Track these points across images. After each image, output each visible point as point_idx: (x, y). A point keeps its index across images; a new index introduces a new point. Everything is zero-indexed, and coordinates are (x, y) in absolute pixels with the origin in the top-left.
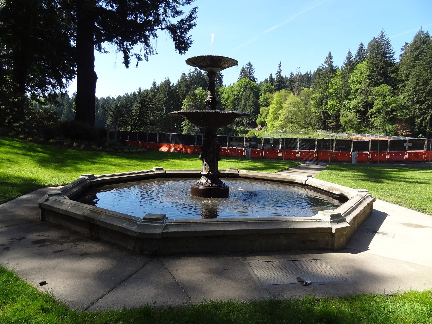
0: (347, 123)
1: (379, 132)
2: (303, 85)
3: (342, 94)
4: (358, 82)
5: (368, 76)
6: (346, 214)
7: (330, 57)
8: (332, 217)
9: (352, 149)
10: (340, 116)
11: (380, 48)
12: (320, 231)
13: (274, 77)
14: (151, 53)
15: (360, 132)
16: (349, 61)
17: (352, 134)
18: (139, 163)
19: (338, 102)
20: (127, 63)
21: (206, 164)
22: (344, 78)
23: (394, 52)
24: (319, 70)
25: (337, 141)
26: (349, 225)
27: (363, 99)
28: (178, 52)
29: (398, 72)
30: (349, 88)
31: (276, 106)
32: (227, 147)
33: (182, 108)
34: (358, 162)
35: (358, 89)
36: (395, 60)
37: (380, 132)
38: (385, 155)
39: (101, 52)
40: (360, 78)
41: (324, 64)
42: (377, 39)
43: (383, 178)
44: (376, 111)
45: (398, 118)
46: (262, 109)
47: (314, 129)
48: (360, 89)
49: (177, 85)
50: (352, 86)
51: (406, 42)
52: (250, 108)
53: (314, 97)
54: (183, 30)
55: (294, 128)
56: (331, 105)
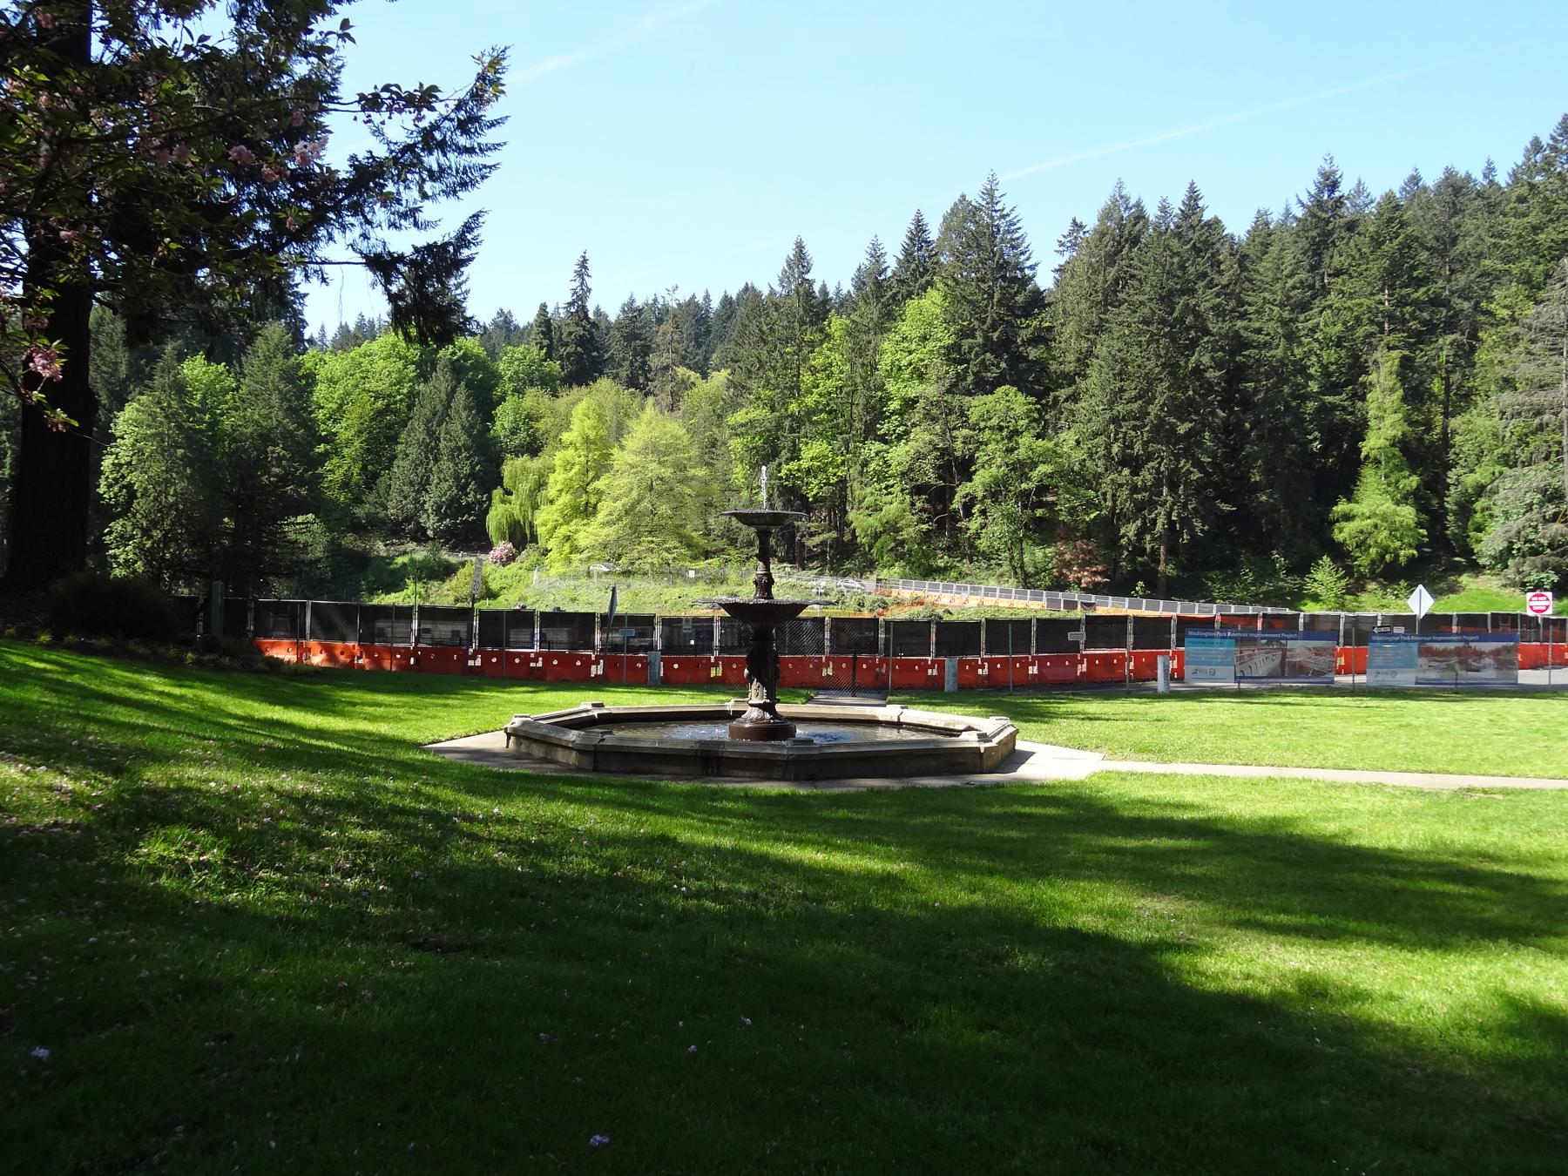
0: (877, 536)
5: (950, 349)
9: (933, 648)
11: (984, 242)
15: (929, 572)
22: (860, 350)
23: (1036, 265)
27: (936, 440)
31: (583, 459)
33: (112, 454)
35: (915, 401)
37: (1001, 575)
38: (1026, 665)
46: (510, 467)
47: (748, 559)
50: (891, 387)
51: (1074, 221)
52: (452, 458)
55: (665, 554)
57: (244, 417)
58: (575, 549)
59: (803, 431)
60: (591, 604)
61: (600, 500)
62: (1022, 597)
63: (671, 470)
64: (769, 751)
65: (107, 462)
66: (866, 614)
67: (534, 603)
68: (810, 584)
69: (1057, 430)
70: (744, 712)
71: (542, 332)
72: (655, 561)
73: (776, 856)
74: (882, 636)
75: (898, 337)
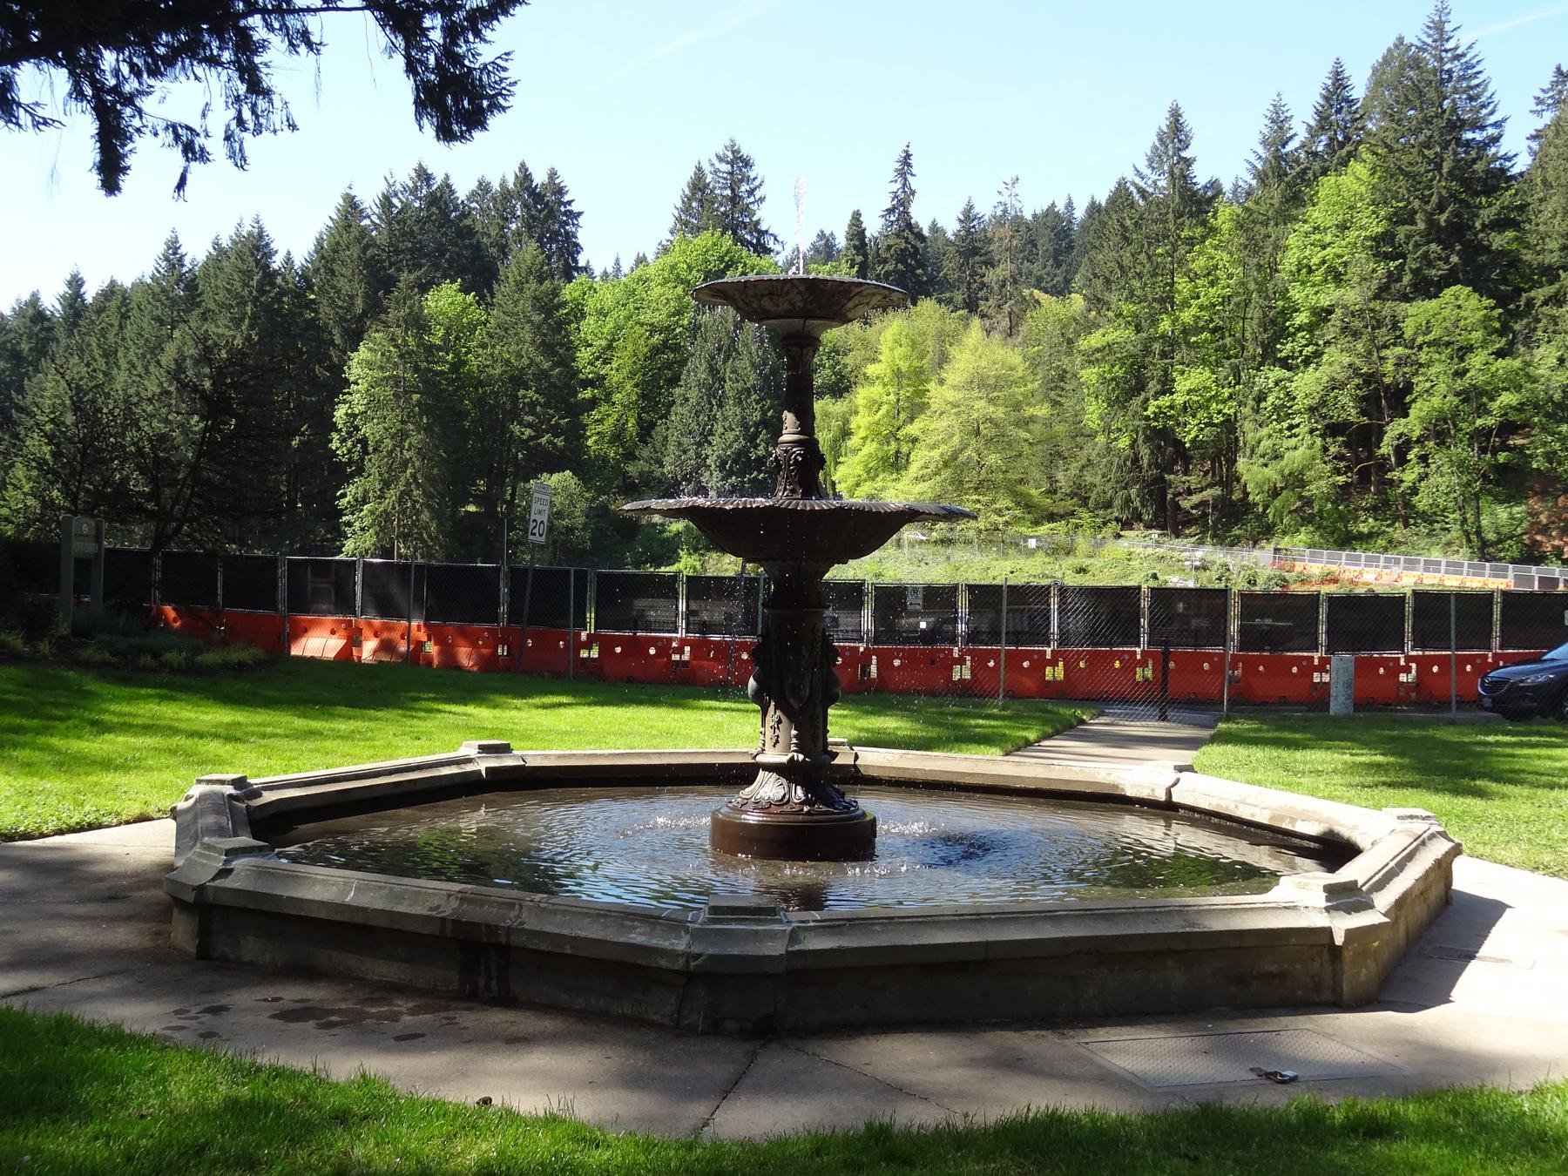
0: (1275, 493)
1: (1444, 540)
2: (1030, 273)
3: (1248, 335)
4: (1328, 272)
5: (1378, 240)
6: (1372, 886)
7: (1176, 133)
8: (1332, 891)
9: (1323, 638)
10: (1237, 451)
11: (1431, 94)
12: (1293, 941)
13: (873, 226)
14: (262, 120)
15: (1346, 541)
16: (1279, 158)
18: (300, 723)
19: (1226, 379)
20: (111, 170)
21: (779, 722)
22: (1254, 247)
23: (1504, 120)
24: (1121, 196)
25: (1254, 603)
26: (1387, 920)
27: (1358, 362)
28: (429, 130)
29: (1527, 227)
30: (1281, 303)
31: (892, 398)
33: (345, 402)
34: (1358, 706)
35: (1329, 311)
36: (1509, 159)
37: (1449, 544)
39: (10, 125)
40: (1339, 251)
41: (1146, 171)
42: (1413, 49)
43: (1483, 776)
44: (1425, 429)
45: (1538, 470)
47: (1105, 524)
48: (1339, 312)
49: (312, 262)
50: (1297, 293)
51: (1558, 68)
53: (1098, 350)
54: (457, 17)
55: (995, 518)
56: (1189, 392)
57: (492, 355)
59: (1178, 357)
65: (340, 413)
69: (1530, 343)
71: (855, 247)
75: (1307, 227)
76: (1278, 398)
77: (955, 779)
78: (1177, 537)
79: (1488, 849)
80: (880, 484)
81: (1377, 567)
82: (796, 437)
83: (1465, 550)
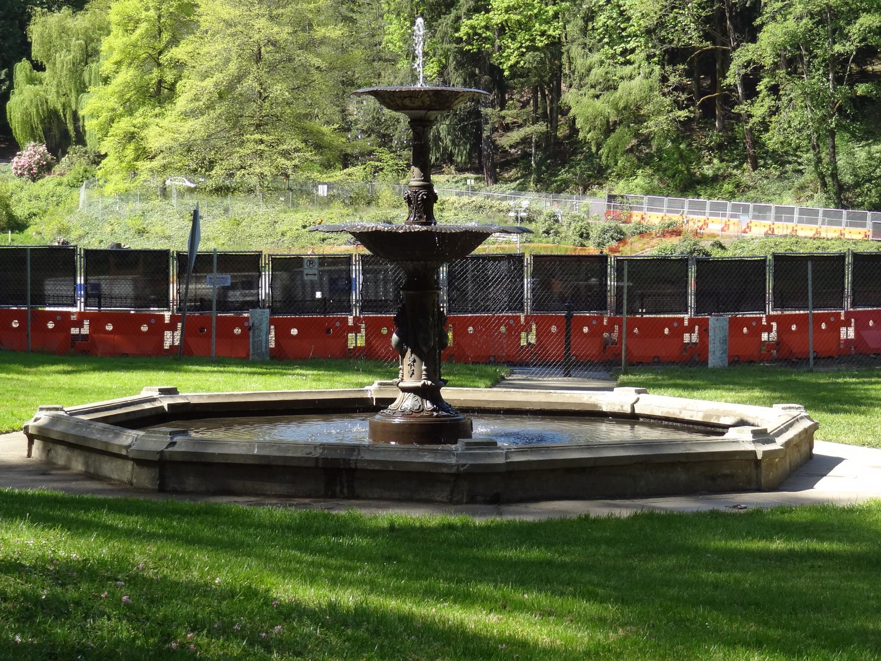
0: (609, 129)
9: (691, 300)
12: (738, 457)
17: (646, 198)
21: (414, 361)
31: (152, 13)
32: (686, 312)
34: (730, 364)
37: (802, 188)
38: (836, 325)
55: (282, 161)
56: (508, 10)
58: (143, 154)
60: (169, 238)
61: (179, 77)
62: (834, 221)
63: (288, 29)
64: (428, 459)
66: (592, 249)
67: (81, 237)
68: (505, 204)
70: (392, 400)
72: (267, 170)
73: (424, 618)
74: (611, 283)
76: (611, 18)
77: (482, 405)
78: (496, 181)
79: (835, 437)
80: (140, 120)
81: (724, 215)
82: (421, 183)
83: (819, 196)
